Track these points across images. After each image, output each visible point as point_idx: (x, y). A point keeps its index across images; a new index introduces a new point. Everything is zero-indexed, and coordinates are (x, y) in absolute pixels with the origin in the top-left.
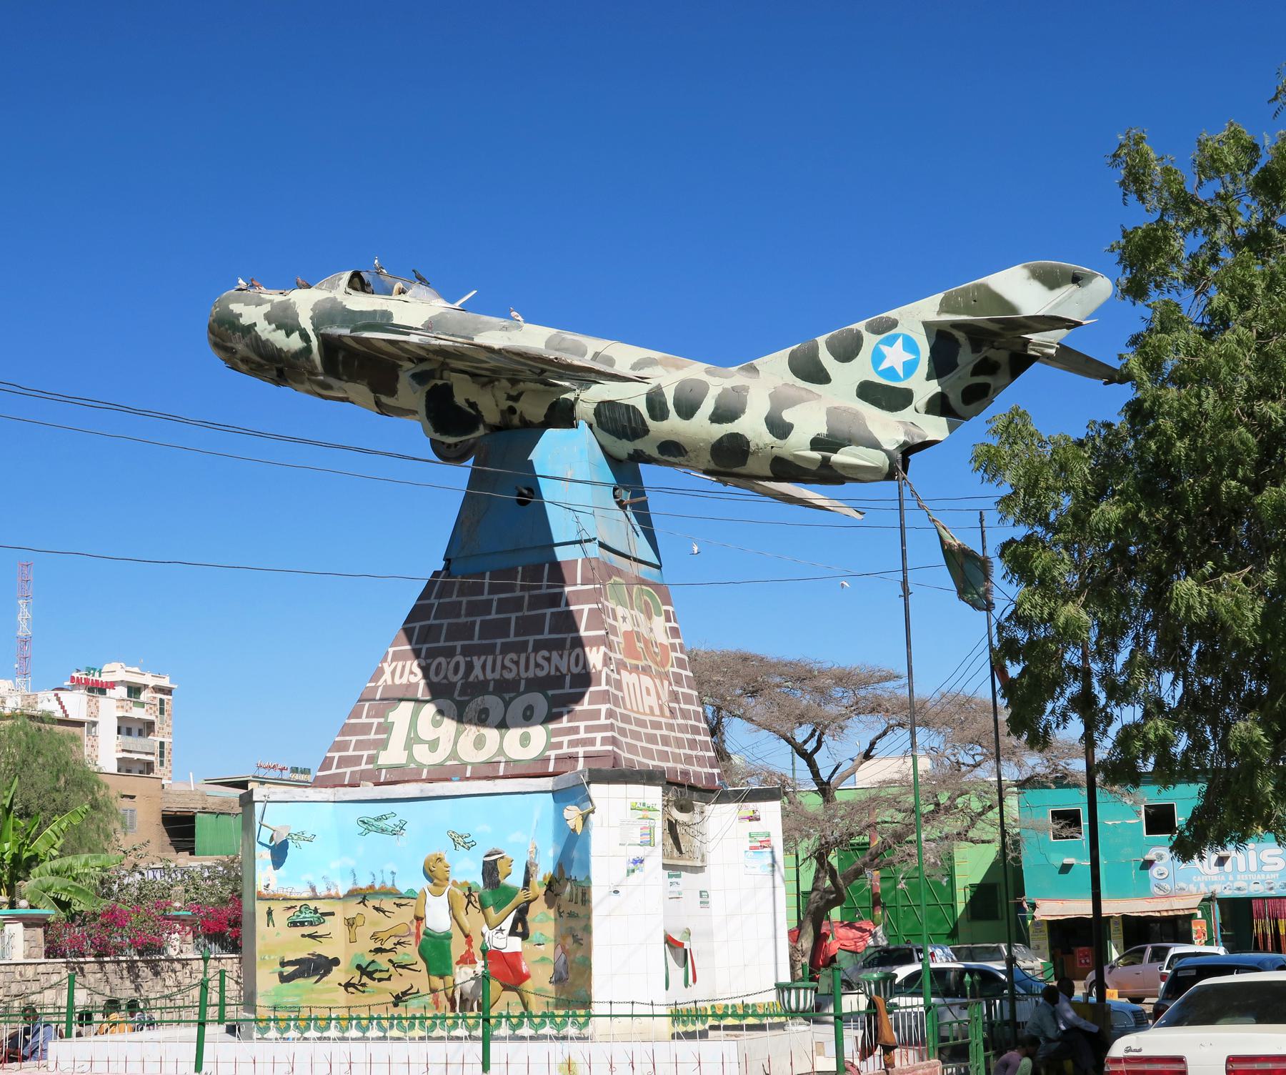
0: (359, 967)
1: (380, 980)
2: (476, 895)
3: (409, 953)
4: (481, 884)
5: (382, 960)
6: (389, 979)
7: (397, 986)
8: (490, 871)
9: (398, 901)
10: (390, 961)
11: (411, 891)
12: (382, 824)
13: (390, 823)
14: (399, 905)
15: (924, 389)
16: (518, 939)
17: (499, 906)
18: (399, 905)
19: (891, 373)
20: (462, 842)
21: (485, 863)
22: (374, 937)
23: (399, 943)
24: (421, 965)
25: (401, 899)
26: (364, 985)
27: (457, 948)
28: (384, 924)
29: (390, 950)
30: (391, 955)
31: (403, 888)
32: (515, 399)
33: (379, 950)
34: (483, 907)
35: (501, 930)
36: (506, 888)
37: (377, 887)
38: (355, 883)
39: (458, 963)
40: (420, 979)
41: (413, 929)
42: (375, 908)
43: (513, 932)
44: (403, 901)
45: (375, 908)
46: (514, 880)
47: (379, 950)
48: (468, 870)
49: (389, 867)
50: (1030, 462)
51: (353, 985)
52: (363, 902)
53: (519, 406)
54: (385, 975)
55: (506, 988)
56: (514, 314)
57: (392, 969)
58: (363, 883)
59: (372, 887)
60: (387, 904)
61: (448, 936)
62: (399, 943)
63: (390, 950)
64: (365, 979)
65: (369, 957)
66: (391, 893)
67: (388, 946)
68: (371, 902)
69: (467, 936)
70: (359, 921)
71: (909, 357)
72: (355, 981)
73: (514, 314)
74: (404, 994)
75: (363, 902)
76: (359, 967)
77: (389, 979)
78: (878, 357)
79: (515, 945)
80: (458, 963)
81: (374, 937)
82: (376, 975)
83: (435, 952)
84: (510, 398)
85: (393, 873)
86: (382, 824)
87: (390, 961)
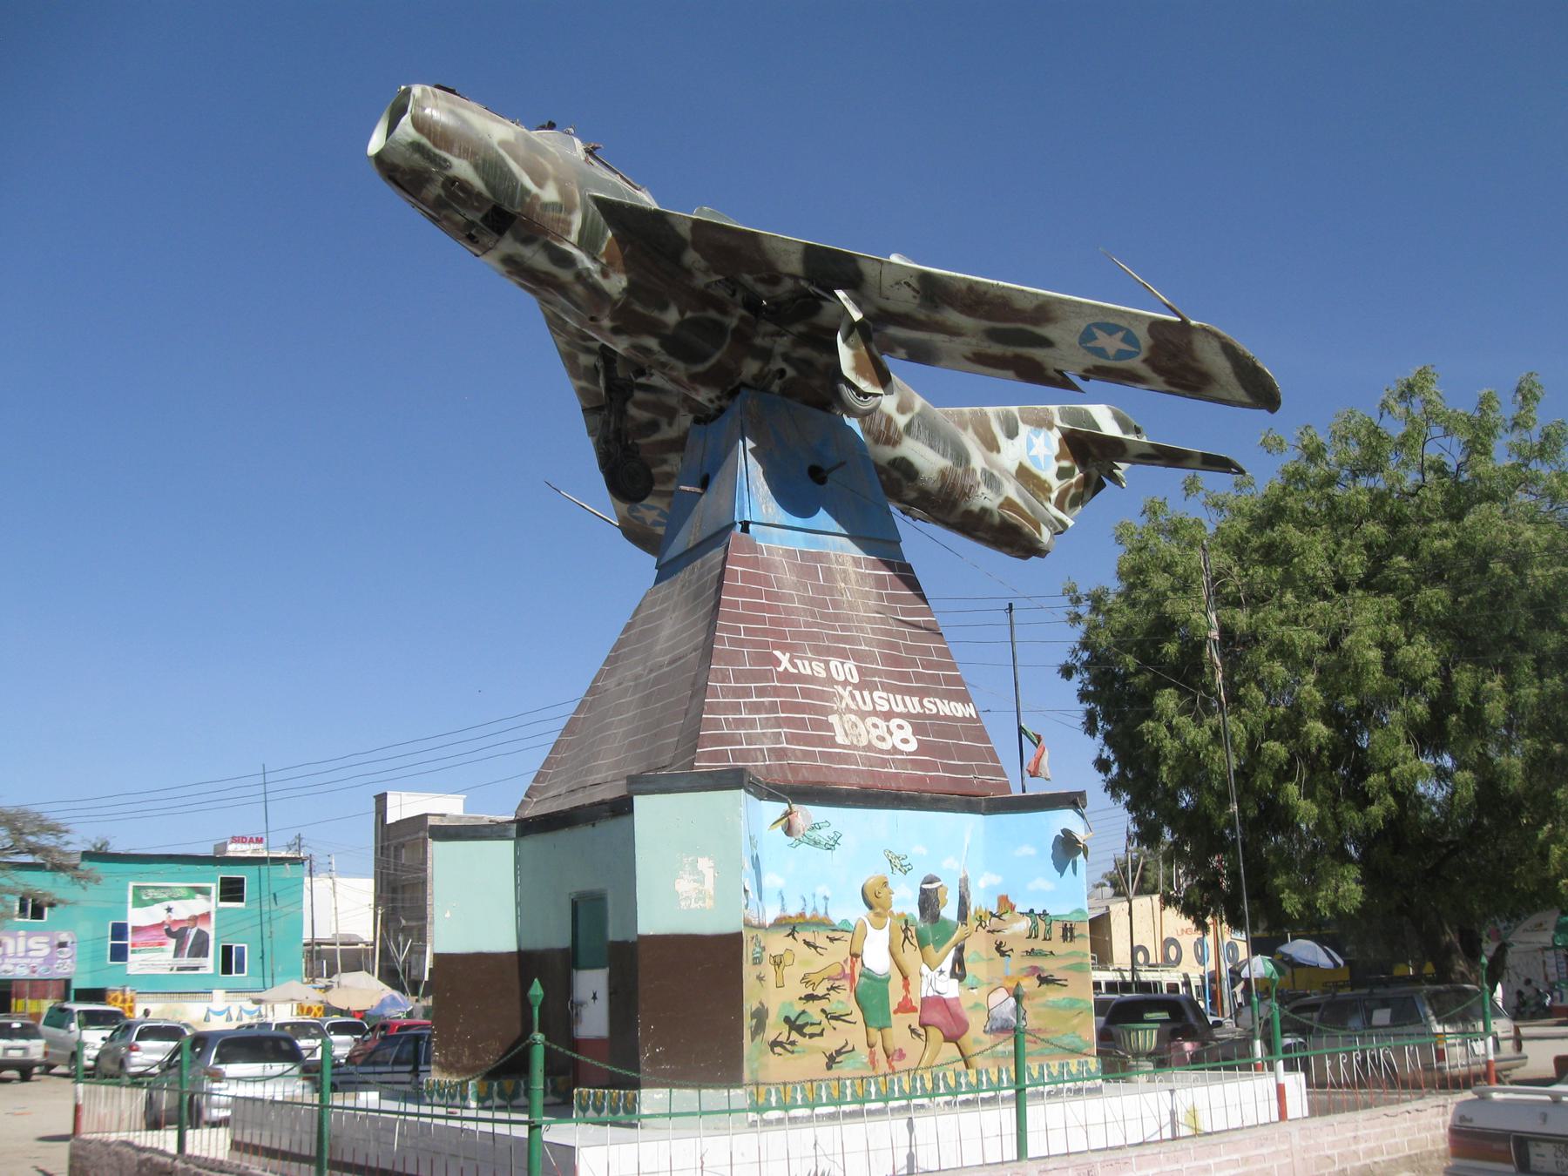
0: (787, 1020)
1: (812, 1036)
2: (913, 929)
3: (843, 1001)
4: (917, 914)
5: (814, 1010)
6: (821, 1034)
7: (830, 1042)
8: (929, 902)
9: (832, 935)
10: (823, 1011)
11: (845, 921)
12: (815, 834)
13: (823, 834)
14: (832, 940)
15: (1056, 485)
16: (956, 981)
17: (938, 944)
18: (832, 940)
19: (1034, 459)
20: (900, 864)
21: (923, 891)
22: (805, 980)
23: (833, 988)
24: (857, 1015)
25: (835, 932)
26: (793, 1043)
27: (895, 996)
28: (818, 963)
29: (823, 997)
30: (823, 1004)
31: (836, 917)
33: (810, 998)
34: (922, 943)
35: (941, 972)
36: (945, 921)
37: (808, 915)
38: (783, 909)
39: (896, 1012)
40: (854, 1034)
41: (848, 971)
42: (806, 942)
43: (953, 974)
44: (837, 935)
45: (807, 944)
46: (949, 911)
47: (810, 998)
48: (905, 901)
49: (822, 890)
51: (781, 1044)
52: (792, 934)
54: (817, 1030)
55: (947, 1039)
57: (825, 1021)
58: (793, 910)
59: (802, 915)
60: (821, 941)
62: (833, 988)
63: (823, 997)
64: (795, 1036)
65: (800, 1006)
66: (822, 923)
67: (820, 991)
68: (800, 936)
69: (905, 978)
70: (788, 959)
72: (783, 1038)
74: (839, 1052)
75: (792, 934)
76: (787, 1020)
77: (821, 1034)
78: (1030, 446)
79: (950, 989)
80: (896, 1012)
81: (805, 980)
83: (871, 997)
85: (826, 898)
86: (815, 834)
87: (823, 1011)
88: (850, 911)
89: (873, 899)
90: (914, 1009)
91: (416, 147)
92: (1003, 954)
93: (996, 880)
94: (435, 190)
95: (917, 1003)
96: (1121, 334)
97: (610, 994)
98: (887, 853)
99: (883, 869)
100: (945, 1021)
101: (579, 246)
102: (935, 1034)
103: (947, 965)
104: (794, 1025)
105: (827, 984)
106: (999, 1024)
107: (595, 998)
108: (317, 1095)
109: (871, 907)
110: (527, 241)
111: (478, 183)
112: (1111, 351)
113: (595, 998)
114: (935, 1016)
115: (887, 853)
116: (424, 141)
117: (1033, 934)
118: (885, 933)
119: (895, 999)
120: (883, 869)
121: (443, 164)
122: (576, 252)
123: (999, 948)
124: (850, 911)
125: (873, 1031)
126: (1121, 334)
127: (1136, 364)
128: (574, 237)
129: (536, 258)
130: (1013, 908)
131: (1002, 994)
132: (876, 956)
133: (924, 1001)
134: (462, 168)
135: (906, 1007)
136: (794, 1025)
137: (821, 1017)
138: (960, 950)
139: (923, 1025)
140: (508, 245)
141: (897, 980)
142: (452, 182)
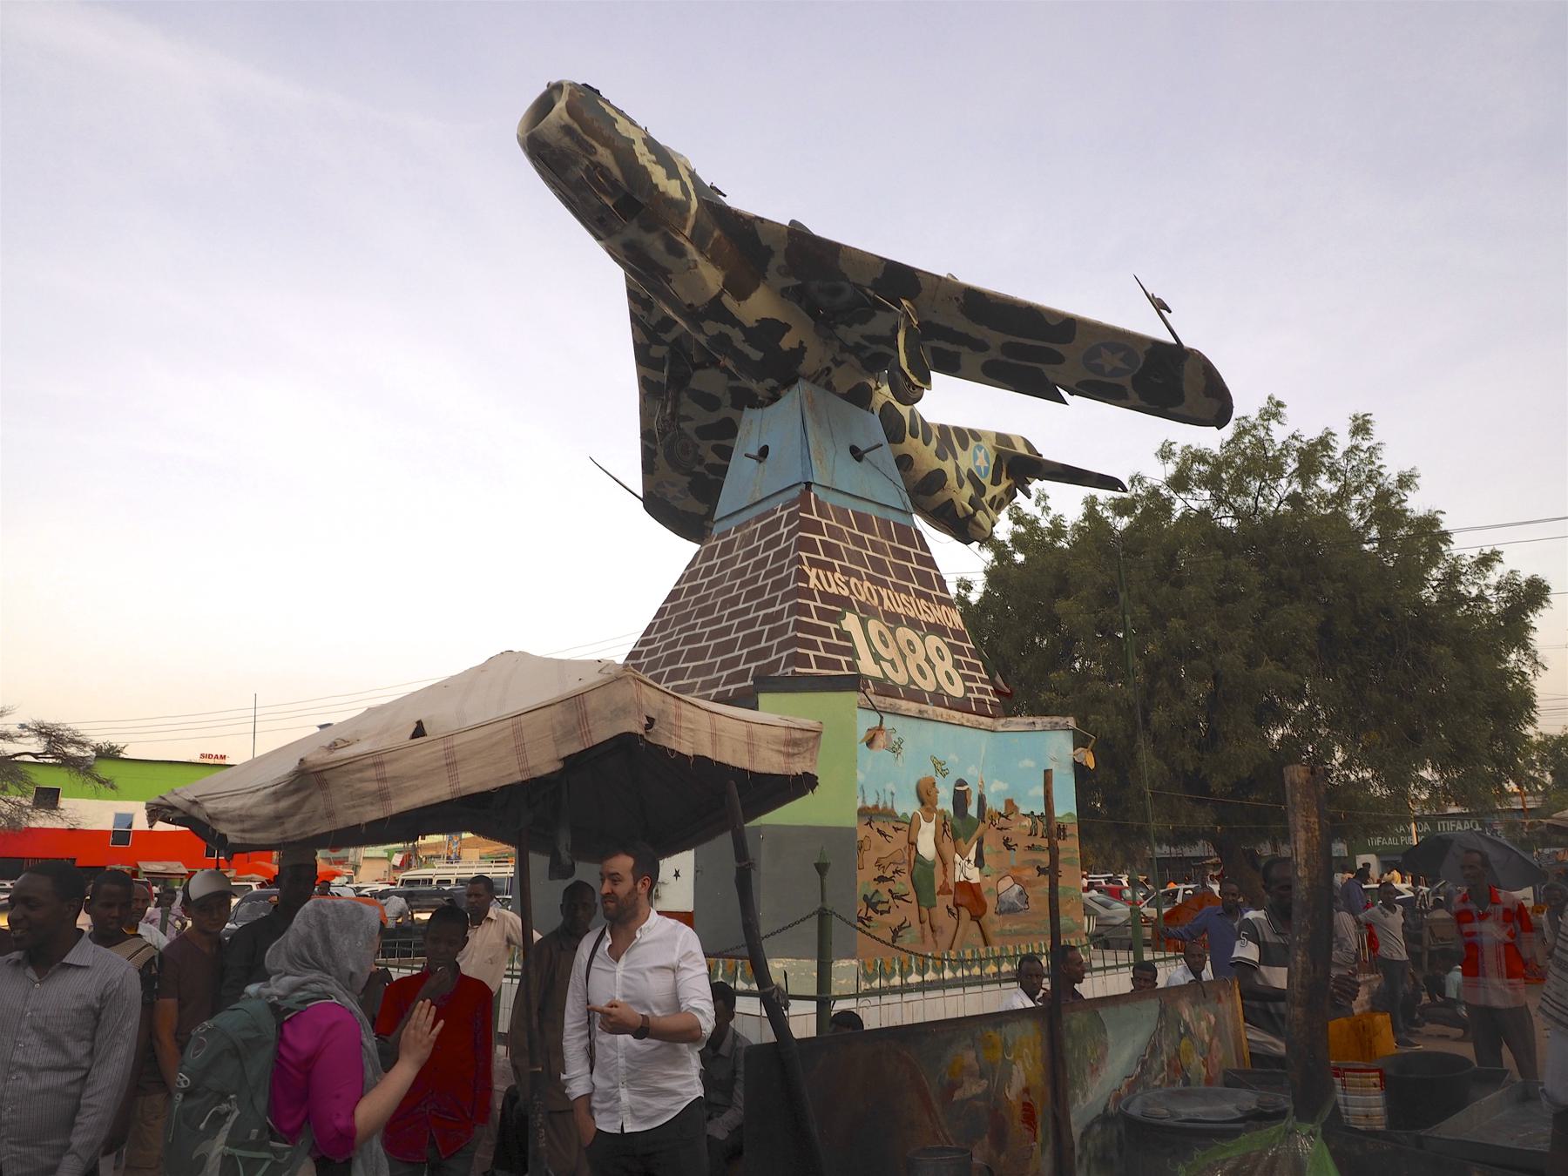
1: (882, 913)
3: (903, 884)
5: (883, 888)
7: (894, 919)
8: (960, 799)
14: (896, 829)
18: (896, 829)
19: (978, 468)
20: (940, 767)
22: (878, 864)
23: (896, 872)
24: (912, 897)
26: (869, 919)
28: (888, 849)
30: (889, 884)
31: (899, 811)
32: (838, 364)
33: (881, 879)
34: (955, 839)
40: (906, 912)
44: (900, 826)
46: (973, 810)
47: (881, 879)
48: (945, 803)
49: (890, 787)
50: (1463, 578)
53: (835, 371)
56: (441, 1023)
58: (870, 803)
59: (876, 807)
61: (933, 865)
62: (896, 872)
64: (871, 913)
65: (873, 887)
67: (888, 874)
68: (877, 824)
71: (1108, 368)
73: (441, 1023)
74: (901, 927)
75: (869, 823)
79: (974, 875)
82: (880, 908)
84: (834, 360)
88: (907, 806)
89: (925, 795)
90: (950, 892)
91: (567, 130)
92: (1009, 848)
93: (1003, 786)
94: (578, 172)
95: (952, 887)
96: (1122, 354)
97: (696, 871)
98: (933, 758)
99: (931, 772)
100: (970, 898)
101: (691, 240)
102: (965, 913)
103: (972, 856)
104: (870, 903)
105: (893, 868)
106: (1006, 907)
107: (677, 875)
108: (777, 978)
109: (923, 804)
110: (649, 228)
111: (616, 172)
112: (1108, 368)
113: (677, 875)
114: (966, 899)
115: (933, 758)
116: (576, 126)
117: (1033, 833)
118: (932, 826)
119: (938, 883)
120: (931, 772)
121: (591, 150)
122: (688, 245)
123: (1006, 842)
124: (907, 806)
125: (924, 909)
126: (1122, 354)
127: (1126, 381)
128: (687, 232)
129: (654, 245)
130: (1016, 809)
131: (1008, 882)
132: (926, 846)
133: (959, 885)
134: (604, 156)
135: (944, 890)
136: (870, 903)
137: (887, 897)
138: (980, 843)
139: (956, 905)
140: (632, 231)
141: (939, 865)
142: (598, 166)
